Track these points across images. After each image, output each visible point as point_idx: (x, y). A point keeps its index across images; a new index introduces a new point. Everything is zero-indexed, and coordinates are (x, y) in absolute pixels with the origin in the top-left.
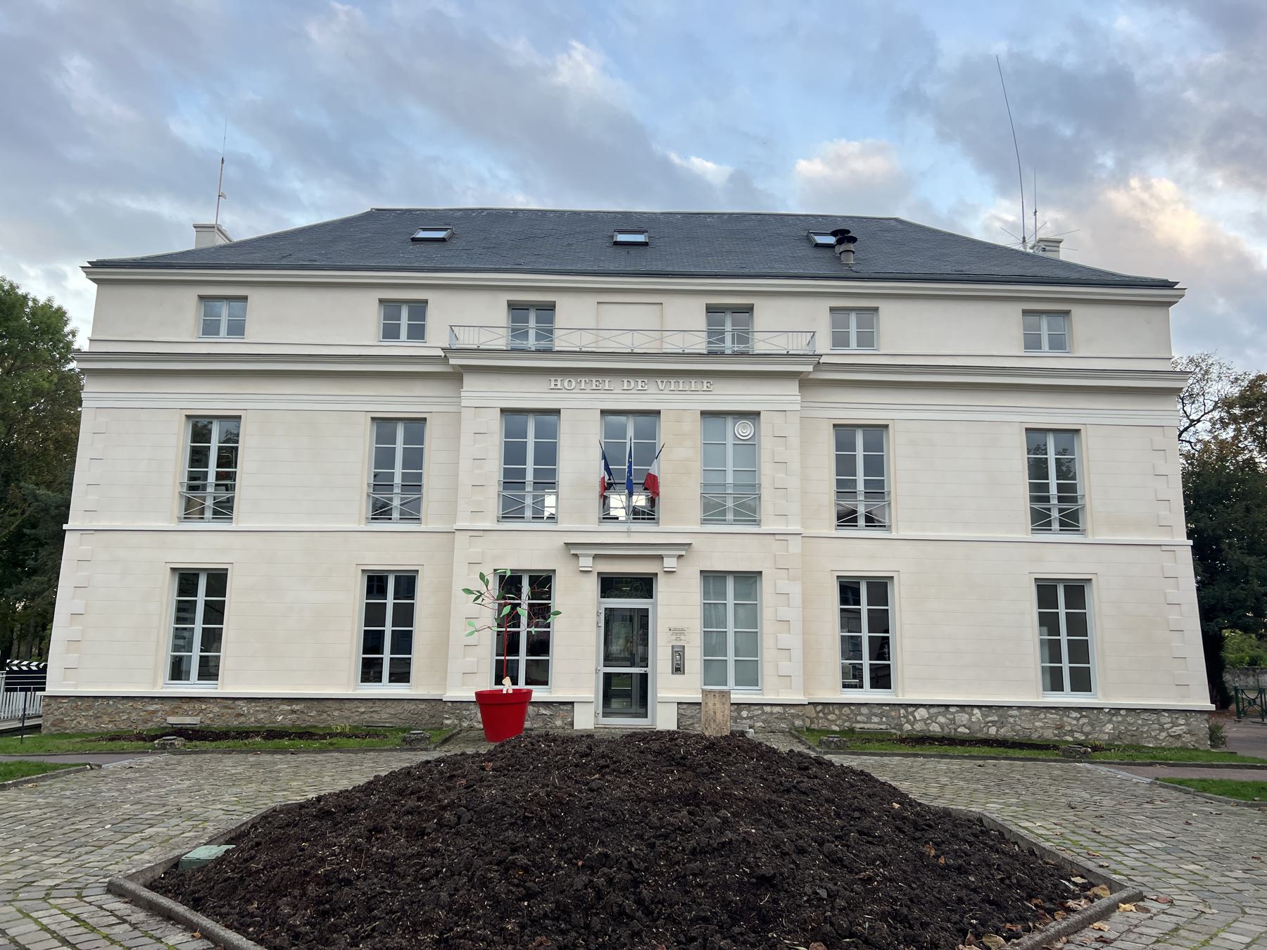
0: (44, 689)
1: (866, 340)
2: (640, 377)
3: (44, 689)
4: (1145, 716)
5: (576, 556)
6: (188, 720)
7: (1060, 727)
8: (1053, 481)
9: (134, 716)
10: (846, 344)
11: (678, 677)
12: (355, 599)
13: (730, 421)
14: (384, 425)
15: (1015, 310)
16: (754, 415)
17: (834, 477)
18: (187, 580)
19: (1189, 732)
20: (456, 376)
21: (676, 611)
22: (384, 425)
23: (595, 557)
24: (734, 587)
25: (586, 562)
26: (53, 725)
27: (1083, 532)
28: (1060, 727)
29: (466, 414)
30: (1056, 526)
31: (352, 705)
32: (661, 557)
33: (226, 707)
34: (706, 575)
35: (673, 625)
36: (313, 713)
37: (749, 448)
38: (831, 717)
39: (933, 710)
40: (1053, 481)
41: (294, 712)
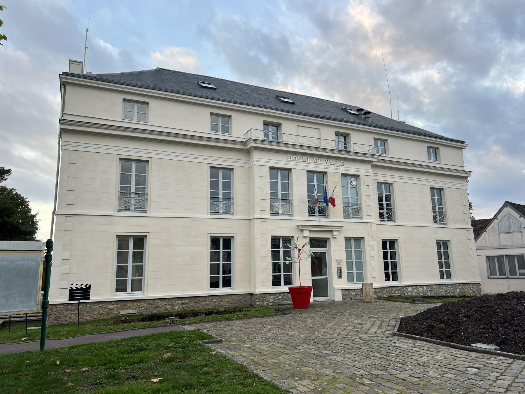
0: (89, 298)
1: (226, 130)
2: (320, 158)
3: (89, 298)
4: (466, 286)
5: (302, 230)
6: (131, 312)
7: (446, 291)
8: (384, 202)
9: (101, 312)
10: (217, 130)
11: (80, 282)
12: (206, 249)
13: (349, 178)
14: (215, 170)
15: (207, 111)
16: (357, 177)
17: (209, 190)
18: (122, 241)
19: (477, 290)
20: (248, 152)
21: (336, 253)
22: (215, 170)
23: (310, 231)
24: (355, 242)
25: (306, 233)
26: (55, 320)
27: (394, 221)
28: (446, 291)
29: (256, 168)
30: (386, 219)
31: (210, 299)
32: (332, 231)
33: (150, 304)
34: (348, 239)
35: (337, 258)
36: (193, 304)
37: (357, 189)
38: (384, 292)
39: (413, 287)
40: (384, 202)
41: (183, 304)
